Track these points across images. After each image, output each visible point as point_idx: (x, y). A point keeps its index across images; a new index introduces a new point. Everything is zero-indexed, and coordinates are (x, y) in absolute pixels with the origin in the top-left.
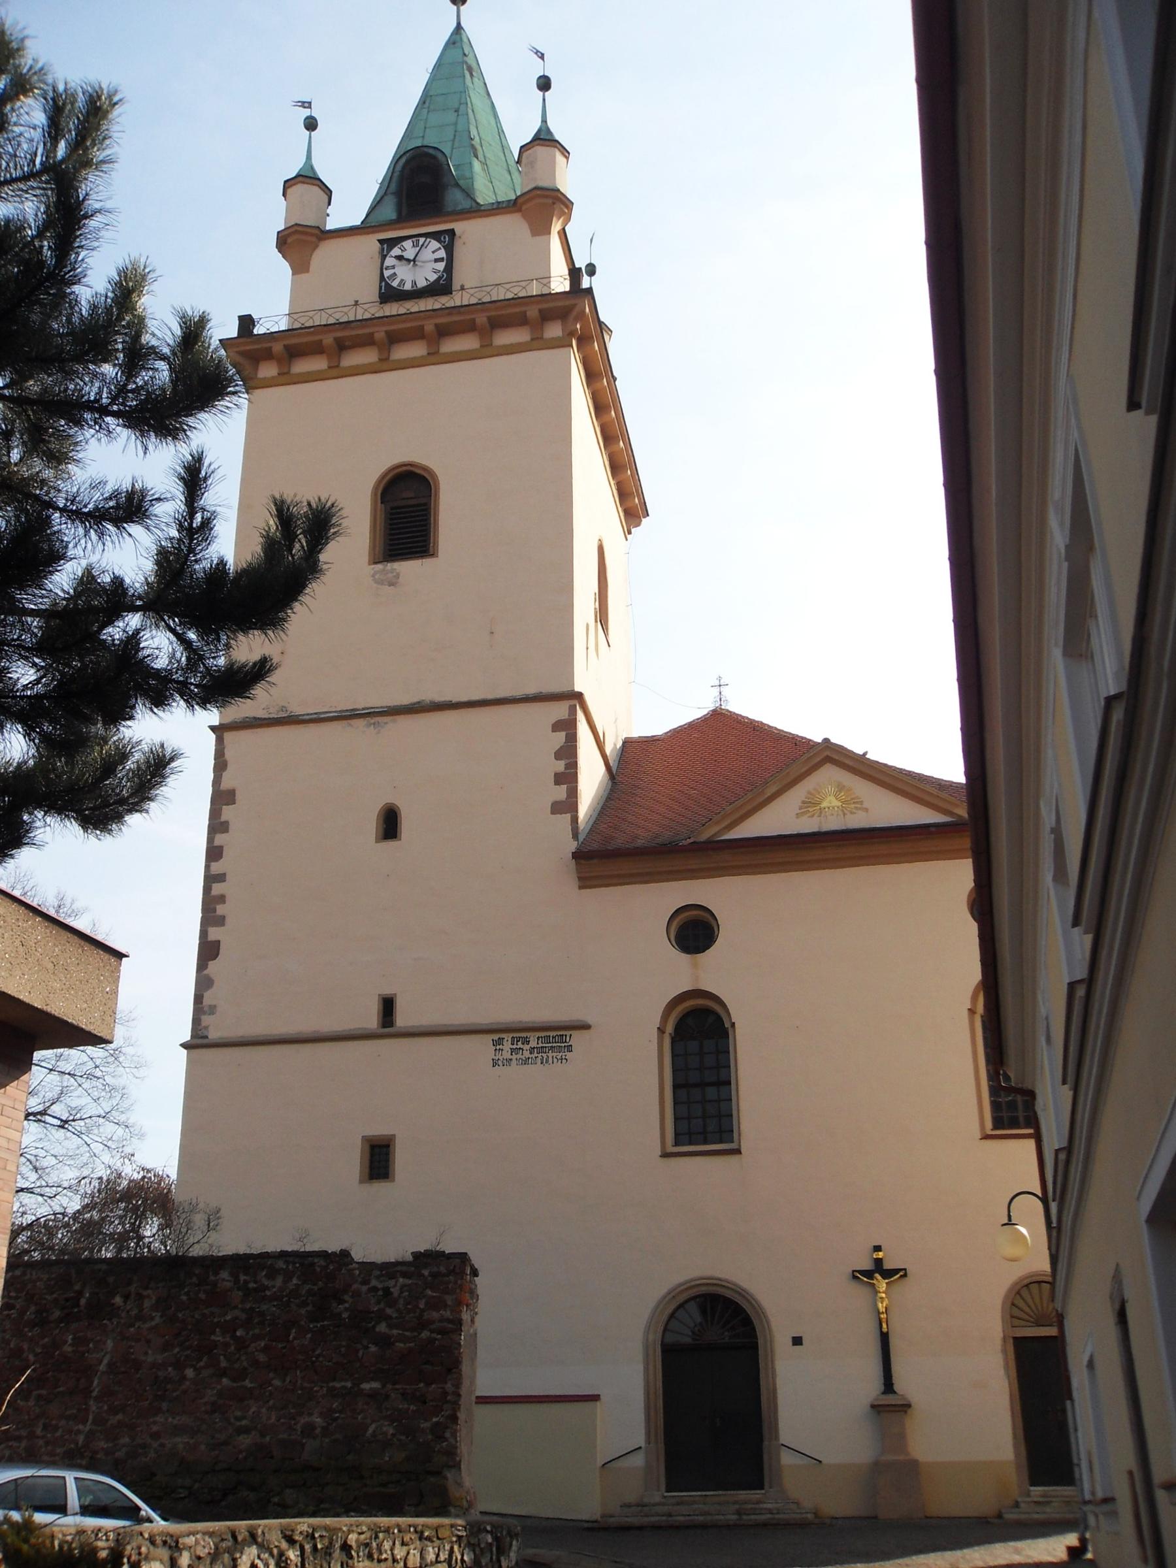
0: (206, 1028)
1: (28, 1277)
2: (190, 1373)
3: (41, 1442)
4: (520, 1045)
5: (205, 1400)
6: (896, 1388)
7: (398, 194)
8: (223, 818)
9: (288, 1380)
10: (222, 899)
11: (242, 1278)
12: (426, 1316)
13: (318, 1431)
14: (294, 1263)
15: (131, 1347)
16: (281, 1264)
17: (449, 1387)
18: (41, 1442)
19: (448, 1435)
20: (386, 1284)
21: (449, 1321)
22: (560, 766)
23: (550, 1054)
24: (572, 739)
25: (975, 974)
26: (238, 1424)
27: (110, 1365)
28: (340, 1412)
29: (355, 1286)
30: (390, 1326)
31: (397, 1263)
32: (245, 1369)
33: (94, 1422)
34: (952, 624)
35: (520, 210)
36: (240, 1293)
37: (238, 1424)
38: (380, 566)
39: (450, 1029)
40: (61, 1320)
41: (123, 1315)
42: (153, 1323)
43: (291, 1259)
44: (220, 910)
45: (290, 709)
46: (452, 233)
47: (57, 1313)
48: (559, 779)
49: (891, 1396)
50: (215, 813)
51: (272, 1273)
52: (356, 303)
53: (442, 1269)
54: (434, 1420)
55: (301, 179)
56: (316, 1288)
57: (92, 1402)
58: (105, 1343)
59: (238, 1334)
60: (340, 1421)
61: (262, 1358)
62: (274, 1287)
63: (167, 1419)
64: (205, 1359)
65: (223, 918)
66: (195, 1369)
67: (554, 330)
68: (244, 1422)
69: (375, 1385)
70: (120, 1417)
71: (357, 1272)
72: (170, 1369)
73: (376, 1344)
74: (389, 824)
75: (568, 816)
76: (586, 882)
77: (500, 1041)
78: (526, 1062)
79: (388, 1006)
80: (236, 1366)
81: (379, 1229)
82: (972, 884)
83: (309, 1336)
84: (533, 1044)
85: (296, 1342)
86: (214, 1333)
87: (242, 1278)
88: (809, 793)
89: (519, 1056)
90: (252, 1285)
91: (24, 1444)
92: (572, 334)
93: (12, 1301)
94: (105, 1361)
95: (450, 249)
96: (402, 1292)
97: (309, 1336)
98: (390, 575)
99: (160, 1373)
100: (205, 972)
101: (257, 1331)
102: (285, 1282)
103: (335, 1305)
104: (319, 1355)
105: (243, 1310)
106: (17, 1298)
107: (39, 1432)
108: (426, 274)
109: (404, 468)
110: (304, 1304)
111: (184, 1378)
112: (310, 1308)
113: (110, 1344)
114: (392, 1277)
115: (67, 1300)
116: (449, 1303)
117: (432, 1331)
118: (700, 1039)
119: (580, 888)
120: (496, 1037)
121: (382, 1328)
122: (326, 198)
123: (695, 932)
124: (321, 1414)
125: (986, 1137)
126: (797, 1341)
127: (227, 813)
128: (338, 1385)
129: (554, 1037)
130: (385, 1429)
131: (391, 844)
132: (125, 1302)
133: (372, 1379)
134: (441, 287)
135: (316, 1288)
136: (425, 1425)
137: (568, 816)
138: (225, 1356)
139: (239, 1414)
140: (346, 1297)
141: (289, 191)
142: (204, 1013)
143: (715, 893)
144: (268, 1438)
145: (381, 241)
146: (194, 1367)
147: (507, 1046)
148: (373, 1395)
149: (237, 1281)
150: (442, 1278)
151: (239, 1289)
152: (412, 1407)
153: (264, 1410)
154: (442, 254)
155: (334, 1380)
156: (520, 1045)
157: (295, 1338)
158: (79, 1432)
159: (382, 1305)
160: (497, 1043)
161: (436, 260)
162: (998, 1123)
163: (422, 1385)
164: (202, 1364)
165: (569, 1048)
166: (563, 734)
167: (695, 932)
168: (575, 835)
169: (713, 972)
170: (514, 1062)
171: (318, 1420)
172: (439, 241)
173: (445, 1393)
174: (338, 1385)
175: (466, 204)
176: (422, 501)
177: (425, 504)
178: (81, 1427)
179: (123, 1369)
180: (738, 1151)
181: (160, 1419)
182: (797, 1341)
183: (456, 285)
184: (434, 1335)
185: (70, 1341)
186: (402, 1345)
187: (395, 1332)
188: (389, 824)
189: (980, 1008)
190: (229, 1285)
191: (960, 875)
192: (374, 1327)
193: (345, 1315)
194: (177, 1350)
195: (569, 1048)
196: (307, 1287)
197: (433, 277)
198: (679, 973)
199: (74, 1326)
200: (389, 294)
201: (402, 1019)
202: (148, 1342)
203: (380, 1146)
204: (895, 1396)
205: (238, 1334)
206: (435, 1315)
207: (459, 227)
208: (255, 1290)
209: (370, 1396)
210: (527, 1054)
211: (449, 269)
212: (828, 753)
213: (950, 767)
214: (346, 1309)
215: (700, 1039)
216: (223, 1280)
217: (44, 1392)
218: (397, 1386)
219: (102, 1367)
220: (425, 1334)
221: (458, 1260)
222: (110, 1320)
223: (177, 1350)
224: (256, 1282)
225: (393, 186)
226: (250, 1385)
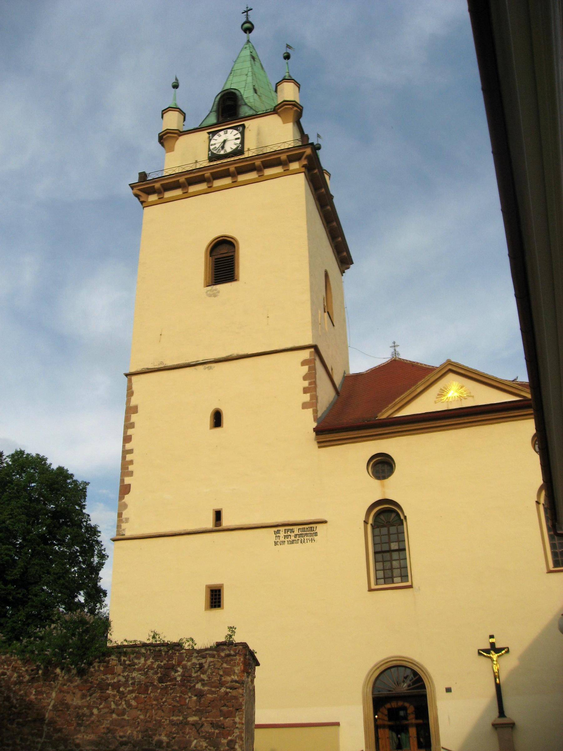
0: (124, 530)
1: (13, 658)
2: (95, 711)
3: (19, 747)
4: (289, 533)
5: (104, 726)
7: (217, 111)
8: (132, 421)
9: (148, 715)
10: (131, 462)
11: (123, 658)
12: (223, 679)
13: (165, 744)
14: (150, 650)
15: (65, 696)
16: (143, 650)
18: (19, 747)
20: (200, 661)
21: (236, 682)
23: (306, 538)
25: (538, 479)
26: (121, 739)
27: (54, 706)
28: (178, 733)
29: (184, 662)
30: (203, 685)
31: (206, 649)
32: (124, 709)
33: (46, 737)
36: (122, 667)
37: (121, 739)
38: (209, 288)
39: (251, 526)
40: (29, 681)
41: (61, 679)
42: (76, 684)
43: (148, 648)
44: (131, 468)
45: (165, 363)
46: (243, 126)
47: (27, 678)
50: (127, 418)
51: (139, 655)
52: (196, 162)
53: (232, 652)
54: (229, 738)
55: (170, 109)
56: (162, 664)
57: (45, 726)
58: (51, 694)
59: (121, 689)
60: (176, 739)
61: (134, 703)
62: (139, 663)
63: (83, 736)
64: (103, 704)
65: (132, 472)
66: (98, 709)
68: (124, 739)
69: (196, 718)
70: (59, 734)
71: (185, 654)
72: (85, 709)
73: (196, 696)
74: (217, 419)
76: (322, 444)
77: (278, 532)
78: (292, 542)
79: (218, 515)
80: (120, 707)
81: (203, 631)
82: (534, 431)
83: (159, 691)
84: (296, 532)
85: (152, 695)
86: (108, 689)
87: (123, 658)
88: (441, 389)
89: (289, 539)
90: (127, 662)
91: (10, 748)
93: (5, 671)
94: (52, 704)
95: (243, 134)
96: (209, 666)
97: (159, 691)
98: (215, 292)
99: (80, 711)
100: (123, 501)
101: (131, 688)
102: (146, 660)
103: (173, 673)
104: (165, 701)
105: (123, 676)
106: (8, 669)
107: (18, 741)
108: (230, 147)
109: (221, 238)
110: (156, 673)
111: (92, 714)
112: (159, 675)
113: (54, 695)
114: (204, 657)
115: (32, 670)
116: (236, 671)
117: (227, 688)
118: (386, 520)
119: (319, 447)
120: (276, 529)
121: (199, 686)
122: (182, 117)
123: (382, 466)
124: (166, 735)
125: (550, 572)
126: (448, 690)
127: (134, 418)
128: (175, 718)
129: (307, 528)
130: (201, 743)
131: (218, 430)
132: (62, 671)
133: (195, 715)
134: (239, 151)
135: (162, 664)
136: (224, 741)
138: (114, 702)
139: (121, 734)
140: (179, 669)
141: (165, 115)
142: (123, 522)
143: (389, 446)
144: (137, 748)
145: (209, 133)
146: (97, 707)
147: (282, 534)
148: (194, 724)
149: (119, 660)
150: (239, 658)
151: (121, 665)
152: (217, 731)
153: (135, 733)
154: (239, 136)
155: (173, 716)
156: (289, 533)
157: (151, 692)
158: (38, 742)
159: (199, 673)
160: (276, 533)
161: (237, 139)
162: (556, 563)
163: (222, 718)
164: (102, 706)
165: (316, 534)
167: (382, 466)
168: (316, 419)
169: (393, 489)
170: (286, 542)
171: (164, 738)
172: (237, 130)
173: (235, 723)
174: (175, 718)
175: (251, 112)
176: (230, 254)
177: (233, 256)
178: (39, 740)
179: (61, 709)
180: (411, 587)
181: (80, 736)
183: (246, 149)
184: (228, 690)
185: (34, 693)
186: (210, 696)
187: (206, 688)
188: (217, 419)
189: (542, 501)
190: (114, 662)
191: (527, 427)
192: (195, 686)
193: (179, 679)
194: (89, 698)
195: (316, 534)
196: (157, 663)
197: (234, 147)
198: (375, 490)
199: (36, 684)
200: (213, 157)
201: (226, 522)
202: (74, 693)
203: (216, 591)
205: (121, 689)
206: (229, 679)
207: (247, 123)
208: (129, 665)
209: (193, 725)
210: (293, 538)
211: (242, 143)
212: (450, 367)
213: (524, 378)
214: (179, 675)
215: (386, 520)
216: (113, 659)
217: (21, 720)
218: (208, 719)
219: (50, 707)
220: (223, 690)
221: (241, 647)
222: (54, 681)
223: (89, 698)
224: (130, 661)
225: (215, 108)
226: (127, 718)
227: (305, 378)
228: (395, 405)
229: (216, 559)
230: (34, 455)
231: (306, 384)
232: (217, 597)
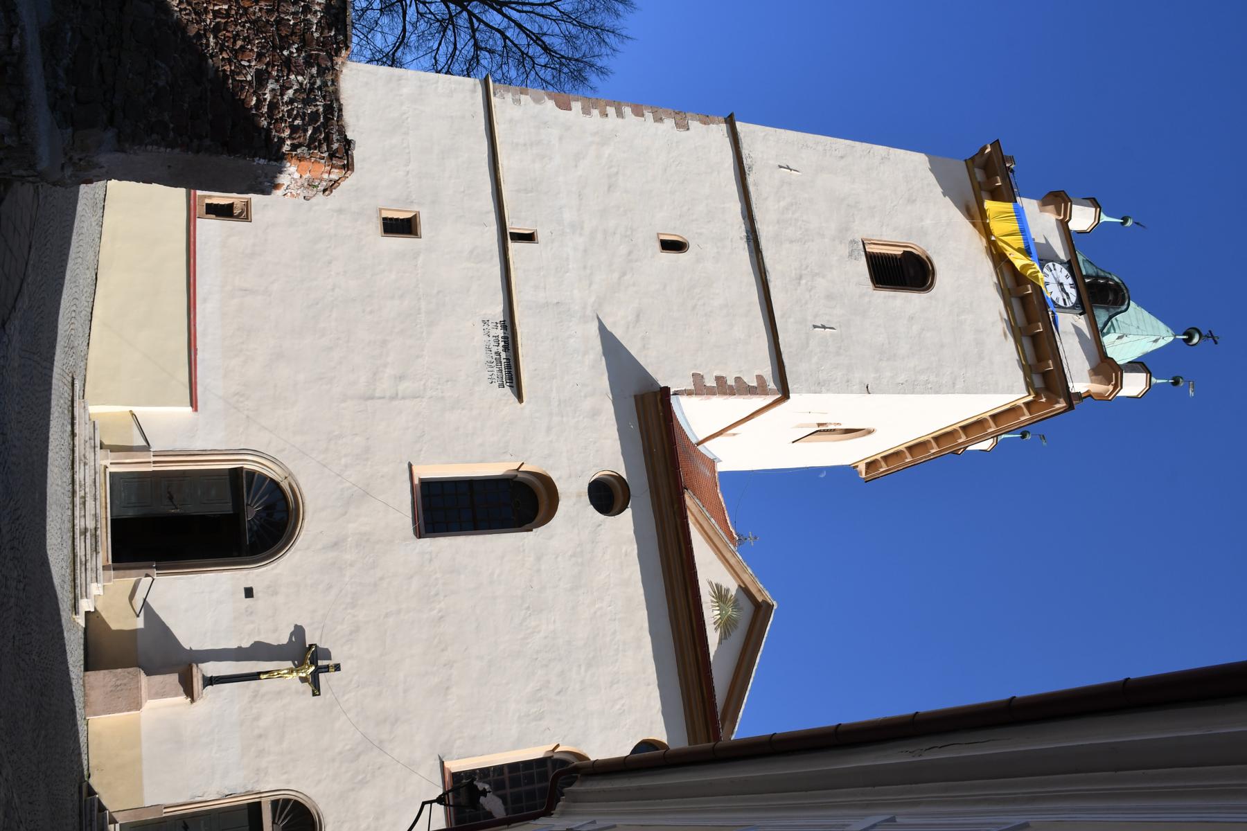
6: (209, 687)
17: (207, 142)
19: (154, 136)
22: (731, 382)
23: (496, 369)
24: (751, 391)
25: (597, 753)
34: (911, 712)
35: (1102, 361)
48: (720, 380)
49: (201, 682)
67: (1038, 382)
75: (692, 387)
92: (1037, 395)
118: (515, 503)
119: (635, 397)
123: (606, 496)
126: (249, 593)
137: (692, 387)
166: (755, 384)
167: (606, 496)
182: (249, 593)
201: (513, 247)
204: (200, 686)
210: (494, 349)
215: (515, 503)
227: (738, 379)
228: (708, 520)
229: (459, 234)
230: (577, 106)
231: (731, 382)
232: (535, 771)
